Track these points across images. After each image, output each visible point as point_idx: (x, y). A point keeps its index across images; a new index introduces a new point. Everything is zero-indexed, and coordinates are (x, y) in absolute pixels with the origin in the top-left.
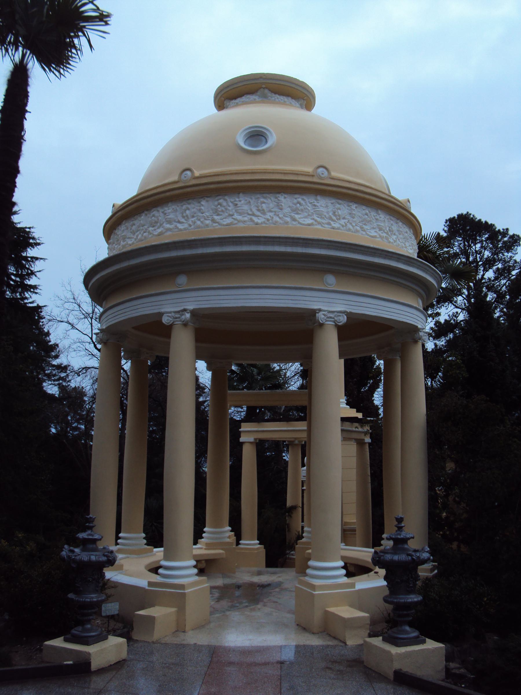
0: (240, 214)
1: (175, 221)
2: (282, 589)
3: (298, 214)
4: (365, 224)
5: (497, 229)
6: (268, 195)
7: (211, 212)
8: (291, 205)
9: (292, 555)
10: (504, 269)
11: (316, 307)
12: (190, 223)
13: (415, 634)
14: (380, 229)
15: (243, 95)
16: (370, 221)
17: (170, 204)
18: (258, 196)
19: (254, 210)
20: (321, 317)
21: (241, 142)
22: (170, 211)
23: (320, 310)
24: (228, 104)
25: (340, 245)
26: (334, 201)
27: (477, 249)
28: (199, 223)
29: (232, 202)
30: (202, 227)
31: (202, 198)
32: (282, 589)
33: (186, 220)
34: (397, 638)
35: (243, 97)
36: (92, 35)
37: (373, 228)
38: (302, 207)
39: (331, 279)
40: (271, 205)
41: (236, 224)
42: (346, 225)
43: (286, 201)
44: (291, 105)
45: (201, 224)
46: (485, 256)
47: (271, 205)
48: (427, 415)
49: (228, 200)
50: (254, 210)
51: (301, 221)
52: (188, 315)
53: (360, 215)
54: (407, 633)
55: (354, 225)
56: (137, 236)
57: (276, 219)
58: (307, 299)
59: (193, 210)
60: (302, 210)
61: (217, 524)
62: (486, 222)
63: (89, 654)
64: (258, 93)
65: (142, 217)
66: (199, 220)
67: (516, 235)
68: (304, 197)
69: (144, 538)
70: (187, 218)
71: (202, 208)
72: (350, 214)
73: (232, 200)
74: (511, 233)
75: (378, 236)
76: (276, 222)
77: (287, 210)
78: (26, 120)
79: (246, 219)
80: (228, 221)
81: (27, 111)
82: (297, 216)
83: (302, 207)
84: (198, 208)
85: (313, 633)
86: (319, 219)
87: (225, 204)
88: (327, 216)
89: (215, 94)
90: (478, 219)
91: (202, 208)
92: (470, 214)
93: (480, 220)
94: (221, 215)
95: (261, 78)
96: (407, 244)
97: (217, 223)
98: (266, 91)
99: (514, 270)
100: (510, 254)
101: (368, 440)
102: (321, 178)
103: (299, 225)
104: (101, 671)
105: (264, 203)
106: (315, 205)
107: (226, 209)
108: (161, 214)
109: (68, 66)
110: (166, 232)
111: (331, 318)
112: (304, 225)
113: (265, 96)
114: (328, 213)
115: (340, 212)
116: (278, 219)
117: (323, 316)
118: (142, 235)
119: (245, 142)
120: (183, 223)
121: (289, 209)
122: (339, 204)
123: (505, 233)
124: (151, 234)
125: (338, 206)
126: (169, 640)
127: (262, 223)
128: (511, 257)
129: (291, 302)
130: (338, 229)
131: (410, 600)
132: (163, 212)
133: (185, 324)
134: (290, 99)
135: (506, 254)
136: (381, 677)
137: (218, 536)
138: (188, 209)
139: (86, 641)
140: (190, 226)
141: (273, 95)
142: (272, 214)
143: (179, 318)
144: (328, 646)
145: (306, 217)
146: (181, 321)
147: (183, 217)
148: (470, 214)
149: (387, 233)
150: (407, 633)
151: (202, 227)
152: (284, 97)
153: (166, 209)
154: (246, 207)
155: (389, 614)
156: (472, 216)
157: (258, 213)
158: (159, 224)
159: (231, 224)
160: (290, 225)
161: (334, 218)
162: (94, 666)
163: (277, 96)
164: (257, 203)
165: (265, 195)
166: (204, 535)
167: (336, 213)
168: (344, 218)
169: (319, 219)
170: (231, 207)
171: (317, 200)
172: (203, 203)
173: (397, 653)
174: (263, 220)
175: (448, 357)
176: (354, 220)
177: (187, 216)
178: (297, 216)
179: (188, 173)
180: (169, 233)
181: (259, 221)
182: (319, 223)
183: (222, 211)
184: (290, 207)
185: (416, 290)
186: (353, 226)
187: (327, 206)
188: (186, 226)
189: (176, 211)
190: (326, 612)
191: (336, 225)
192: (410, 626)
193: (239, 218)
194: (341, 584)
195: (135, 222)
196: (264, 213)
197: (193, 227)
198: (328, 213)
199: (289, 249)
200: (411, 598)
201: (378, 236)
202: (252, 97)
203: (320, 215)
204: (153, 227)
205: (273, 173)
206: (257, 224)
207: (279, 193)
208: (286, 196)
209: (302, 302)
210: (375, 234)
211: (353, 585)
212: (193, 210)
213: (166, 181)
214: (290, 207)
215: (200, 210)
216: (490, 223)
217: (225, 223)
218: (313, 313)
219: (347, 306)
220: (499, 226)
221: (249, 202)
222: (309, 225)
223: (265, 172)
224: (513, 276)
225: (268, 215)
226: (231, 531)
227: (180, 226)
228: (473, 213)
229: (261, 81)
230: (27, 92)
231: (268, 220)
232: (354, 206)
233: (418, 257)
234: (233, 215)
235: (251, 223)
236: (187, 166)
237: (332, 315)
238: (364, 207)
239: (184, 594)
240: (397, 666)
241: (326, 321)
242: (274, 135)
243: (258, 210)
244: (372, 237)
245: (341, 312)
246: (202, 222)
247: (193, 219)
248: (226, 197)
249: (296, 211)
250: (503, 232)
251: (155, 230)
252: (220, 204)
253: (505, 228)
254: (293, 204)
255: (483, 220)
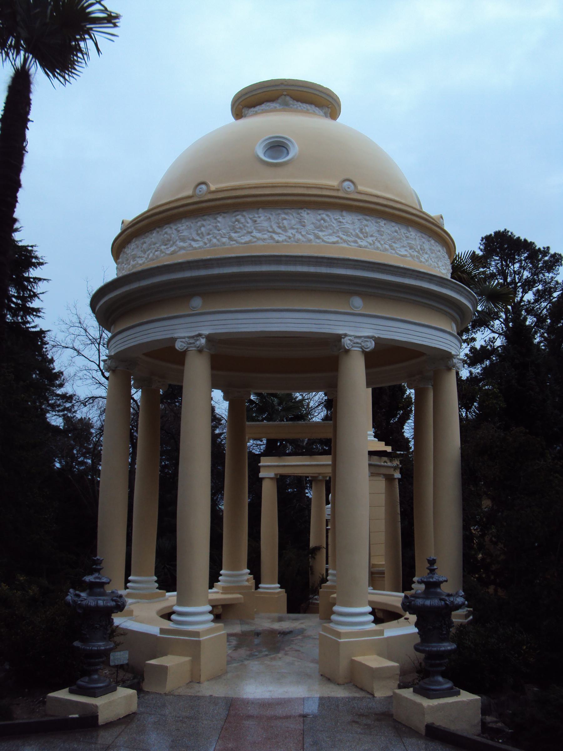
0: (260, 231)
1: (189, 239)
2: (305, 637)
3: (322, 231)
4: (394, 242)
5: (537, 248)
6: (289, 211)
7: (228, 229)
8: (314, 221)
9: (316, 599)
10: (544, 291)
11: (341, 332)
12: (206, 241)
13: (449, 685)
14: (411, 248)
15: (263, 103)
16: (400, 239)
17: (183, 221)
18: (279, 211)
19: (275, 227)
20: (346, 342)
21: (261, 154)
22: (183, 227)
23: (346, 335)
24: (246, 112)
25: (367, 265)
26: (360, 217)
27: (515, 269)
28: (215, 241)
29: (251, 219)
30: (218, 246)
31: (218, 213)
32: (305, 637)
33: (201, 238)
34: (430, 690)
35: (263, 105)
36: (99, 38)
37: (404, 247)
38: (326, 224)
39: (357, 302)
40: (293, 222)
41: (255, 242)
42: (374, 243)
43: (310, 217)
44: (314, 113)
45: (217, 243)
46: (524, 277)
47: (293, 222)
48: (462, 448)
49: (247, 216)
50: (275, 227)
51: (325, 239)
52: (203, 341)
53: (389, 232)
54: (440, 683)
55: (382, 243)
56: (148, 256)
57: (299, 236)
58: (332, 323)
59: (208, 227)
60: (326, 227)
61: (235, 567)
62: (525, 240)
63: (96, 707)
64: (279, 101)
65: (154, 235)
66: (215, 238)
67: (558, 254)
68: (329, 213)
69: (156, 582)
70: (202, 235)
71: (219, 224)
72: (378, 231)
73: (251, 216)
74: (552, 252)
75: (408, 255)
76: (299, 240)
77: (310, 227)
78: (28, 129)
79: (266, 236)
80: (247, 238)
81: (29, 120)
82: (321, 234)
83: (326, 224)
84: (214, 225)
85: (338, 684)
86: (344, 237)
87: (243, 220)
88: (354, 233)
89: (232, 102)
90: (517, 236)
91: (219, 224)
92: (508, 232)
93: (519, 238)
94: (239, 232)
95: (282, 84)
96: (440, 264)
97: (235, 241)
98: (288, 98)
99: (555, 292)
100: (551, 275)
101: (398, 475)
102: (347, 192)
103: (323, 243)
104: (109, 725)
105: (285, 219)
106: (340, 222)
107: (245, 226)
108: (174, 232)
109: (73, 71)
110: (179, 250)
111: (357, 343)
112: (328, 243)
113: (286, 104)
114: (354, 230)
115: (367, 229)
116: (300, 237)
117: (349, 342)
118: (154, 254)
119: (265, 154)
120: (198, 241)
121: (312, 226)
122: (367, 220)
123: (546, 251)
124: (163, 252)
125: (365, 222)
126: (183, 691)
127: (283, 241)
128: (552, 277)
129: (314, 326)
130: (366, 247)
131: (443, 649)
132: (176, 229)
133: (200, 351)
134: (313, 106)
135: (547, 274)
136: (412, 732)
137: (235, 579)
138: (204, 226)
139: (92, 693)
140: (205, 244)
141: (295, 103)
142: (293, 231)
143: (194, 343)
144: (354, 698)
145: (330, 235)
146: (195, 347)
147: (198, 235)
148: (508, 232)
149: (418, 252)
150: (440, 683)
151: (218, 246)
152: (307, 105)
153: (180, 225)
154: (265, 224)
155: (421, 664)
156: (510, 234)
157: (279, 231)
158: (171, 242)
159: (250, 242)
160: (314, 244)
161: (361, 236)
162: (102, 720)
163: (300, 104)
164: (278, 220)
165: (286, 211)
166: (220, 578)
167: (363, 230)
168: (372, 236)
169: (344, 237)
170: (250, 224)
171: (342, 216)
172: (220, 219)
173: (429, 706)
174: (284, 238)
175: (485, 385)
176: (383, 237)
177: (202, 233)
178: (321, 234)
179: (204, 187)
180: (183, 252)
181: (280, 239)
182: (345, 241)
183: (240, 228)
184: (313, 223)
185: (449, 313)
186: (381, 245)
187: (353, 223)
188: (201, 244)
189: (190, 228)
190: (353, 661)
191: (363, 243)
192: (443, 677)
193: (259, 235)
194: (368, 631)
195: (146, 240)
196: (285, 230)
197: (208, 245)
198: (354, 230)
199: (312, 269)
200: (444, 646)
201: (408, 255)
202: (272, 105)
203: (346, 233)
204: (166, 245)
205: (295, 187)
206: (278, 242)
207: (302, 208)
208: (309, 211)
209: (326, 326)
210: (405, 253)
211: (381, 632)
212: (208, 227)
213: (180, 196)
214: (313, 223)
215: (216, 227)
216: (529, 241)
217: (243, 241)
218: (338, 338)
219: (375, 331)
220: (540, 245)
221: (270, 218)
222: (334, 243)
223: (286, 186)
224: (554, 298)
225: (290, 233)
226: (250, 574)
227: (195, 244)
228: (511, 231)
229: (283, 87)
230: (30, 100)
231: (290, 238)
232: (382, 223)
233: (451, 278)
234: (252, 232)
235: (272, 241)
236: (202, 180)
237: (358, 341)
238: (393, 224)
239: (199, 642)
240: (428, 719)
241: (353, 347)
242: (296, 146)
243: (279, 227)
244: (402, 256)
245: (368, 337)
246: (218, 240)
247: (208, 237)
248: (244, 213)
249: (320, 228)
250: (544, 251)
251: (167, 248)
252: (237, 221)
253: (545, 246)
254: (317, 220)
255: (522, 238)
